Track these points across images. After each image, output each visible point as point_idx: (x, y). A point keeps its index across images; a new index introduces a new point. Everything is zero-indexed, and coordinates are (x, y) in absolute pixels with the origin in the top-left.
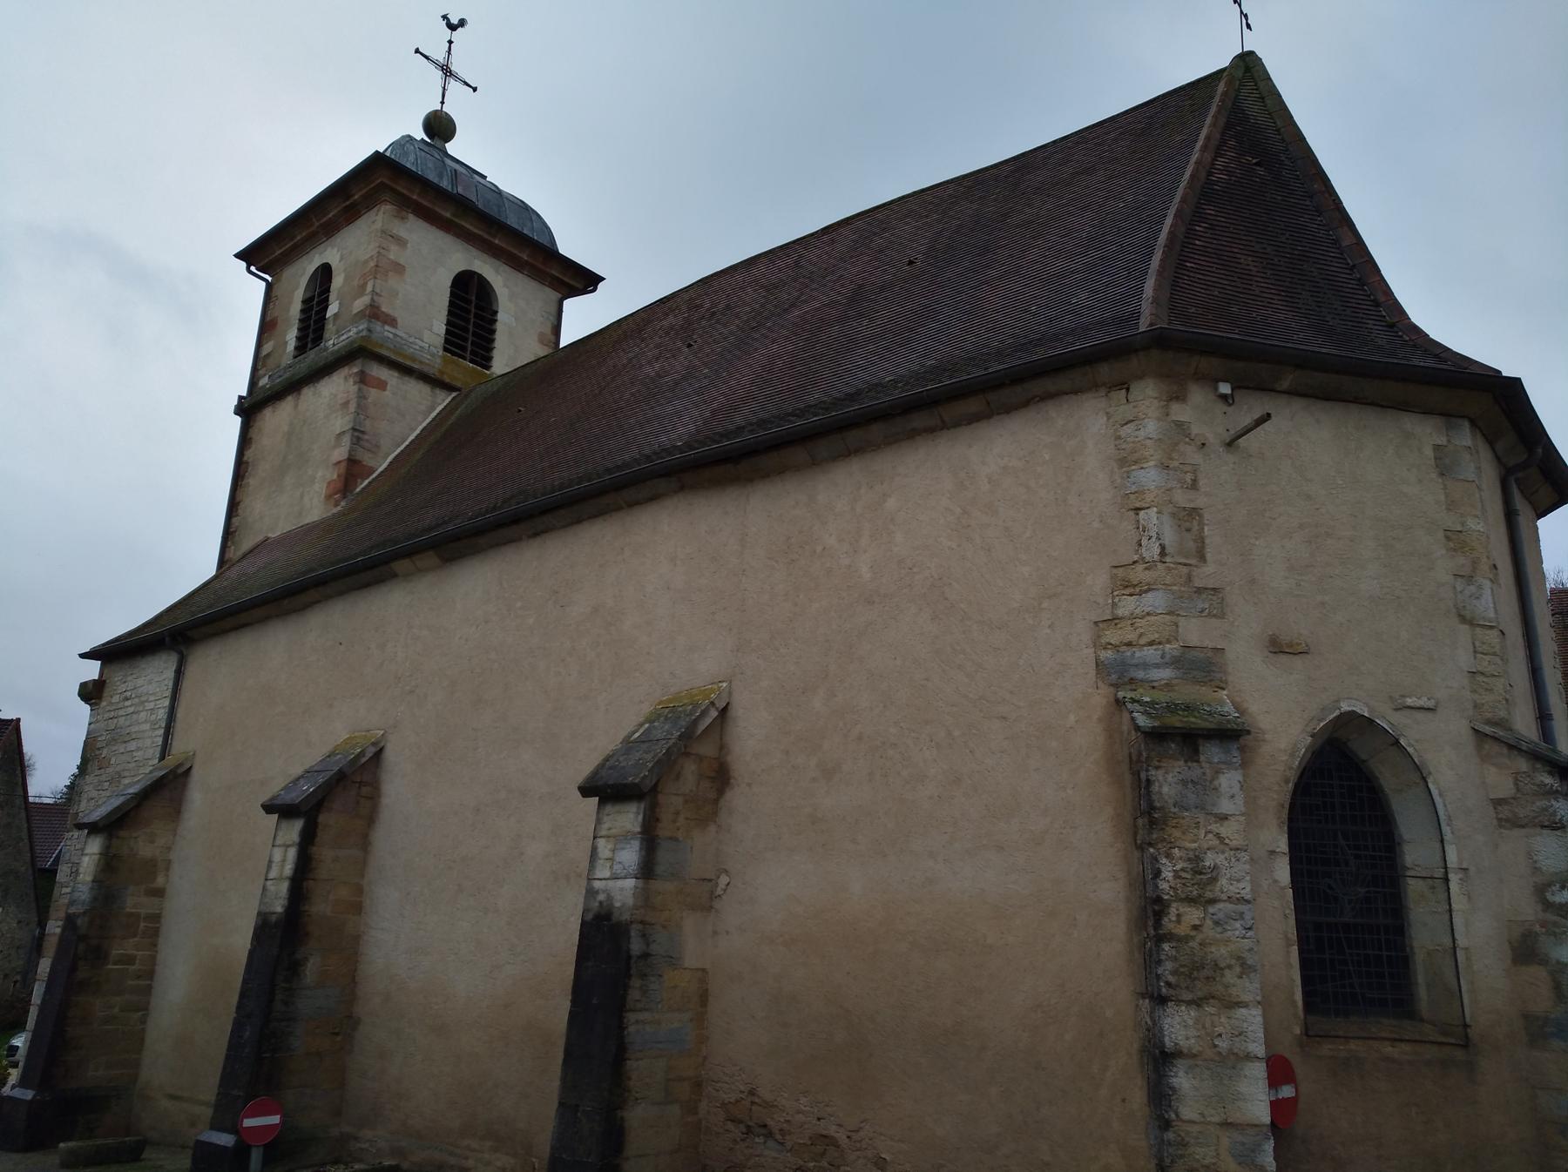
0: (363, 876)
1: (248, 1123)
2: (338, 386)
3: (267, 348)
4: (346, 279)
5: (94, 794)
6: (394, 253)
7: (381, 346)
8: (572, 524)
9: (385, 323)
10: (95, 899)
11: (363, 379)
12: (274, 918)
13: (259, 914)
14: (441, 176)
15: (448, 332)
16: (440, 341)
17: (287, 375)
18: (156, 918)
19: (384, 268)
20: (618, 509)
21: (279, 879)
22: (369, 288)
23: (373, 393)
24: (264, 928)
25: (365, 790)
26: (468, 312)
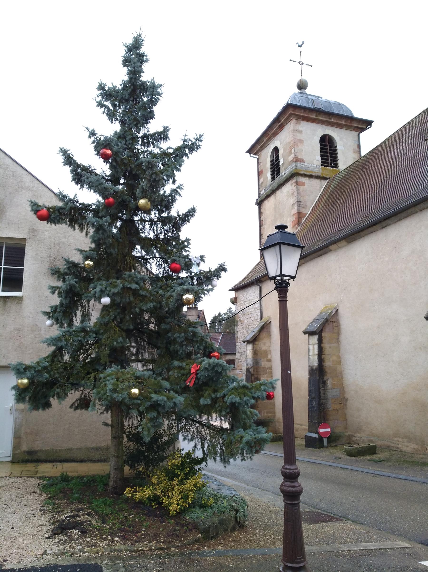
0: (339, 352)
1: (321, 430)
2: (289, 187)
3: (261, 181)
4: (284, 150)
5: (242, 331)
6: (299, 136)
7: (301, 170)
8: (397, 222)
9: (300, 162)
10: (253, 363)
11: (297, 183)
12: (315, 368)
13: (309, 366)
14: (308, 103)
15: (322, 159)
16: (319, 163)
17: (270, 188)
18: (270, 368)
19: (297, 142)
20: (416, 212)
21: (314, 355)
22: (293, 151)
23: (301, 188)
24: (312, 371)
25: (335, 324)
26: (327, 149)
